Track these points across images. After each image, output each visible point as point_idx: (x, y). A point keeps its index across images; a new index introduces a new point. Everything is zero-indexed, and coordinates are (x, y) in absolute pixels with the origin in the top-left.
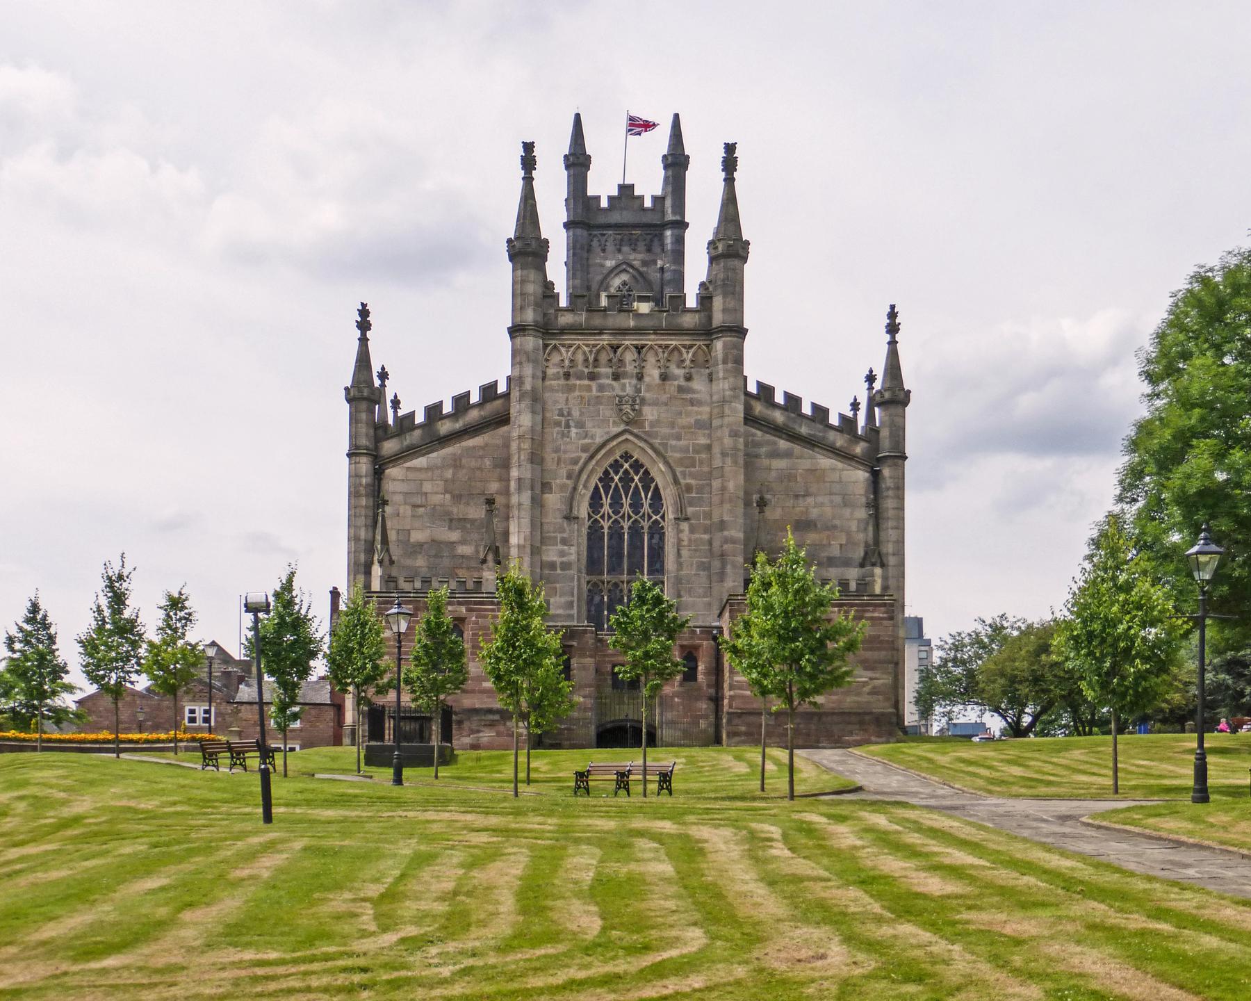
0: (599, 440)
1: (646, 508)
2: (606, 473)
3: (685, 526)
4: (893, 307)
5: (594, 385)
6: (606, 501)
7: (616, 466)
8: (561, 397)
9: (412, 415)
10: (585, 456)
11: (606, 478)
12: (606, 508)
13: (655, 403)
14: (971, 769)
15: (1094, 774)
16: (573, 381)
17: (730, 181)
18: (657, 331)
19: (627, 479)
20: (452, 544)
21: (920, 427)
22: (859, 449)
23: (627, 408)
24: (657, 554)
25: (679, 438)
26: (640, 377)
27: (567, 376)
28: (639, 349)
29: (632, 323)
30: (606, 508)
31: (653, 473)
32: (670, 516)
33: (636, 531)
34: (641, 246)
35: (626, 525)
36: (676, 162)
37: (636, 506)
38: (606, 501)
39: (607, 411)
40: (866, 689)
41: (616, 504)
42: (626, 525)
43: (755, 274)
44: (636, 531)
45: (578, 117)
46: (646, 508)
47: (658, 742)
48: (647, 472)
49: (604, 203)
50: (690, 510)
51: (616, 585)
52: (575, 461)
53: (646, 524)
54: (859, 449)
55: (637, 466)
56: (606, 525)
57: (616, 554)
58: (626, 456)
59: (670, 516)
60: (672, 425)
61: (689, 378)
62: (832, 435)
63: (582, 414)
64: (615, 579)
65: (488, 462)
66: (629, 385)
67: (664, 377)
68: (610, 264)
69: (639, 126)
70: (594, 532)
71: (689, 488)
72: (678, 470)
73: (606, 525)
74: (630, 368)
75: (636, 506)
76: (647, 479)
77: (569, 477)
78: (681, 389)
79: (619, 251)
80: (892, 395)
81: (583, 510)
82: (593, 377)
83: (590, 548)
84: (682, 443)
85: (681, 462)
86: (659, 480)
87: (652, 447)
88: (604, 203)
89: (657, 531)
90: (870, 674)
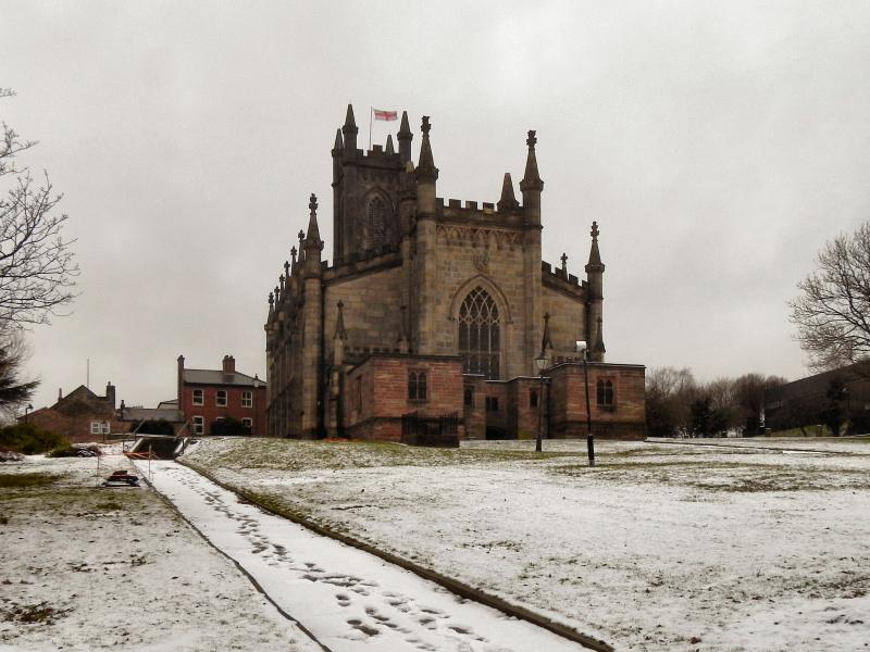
0: (466, 279)
1: (490, 316)
2: (468, 296)
3: (511, 326)
4: (595, 223)
5: (463, 249)
6: (469, 311)
7: (474, 293)
8: (446, 254)
9: (326, 262)
10: (458, 287)
11: (468, 299)
12: (469, 315)
13: (494, 261)
14: (631, 460)
15: (849, 455)
16: (451, 247)
17: (532, 150)
18: (497, 224)
19: (479, 300)
20: (365, 331)
21: (608, 281)
22: (579, 293)
23: (481, 263)
24: (496, 340)
25: (507, 280)
26: (487, 247)
27: (448, 243)
28: (487, 232)
29: (483, 219)
30: (469, 315)
31: (494, 298)
32: (502, 320)
33: (484, 326)
34: (386, 179)
35: (480, 324)
36: (405, 136)
37: (484, 314)
38: (469, 311)
39: (469, 264)
40: (632, 412)
41: (474, 312)
42: (480, 324)
43: (546, 198)
44: (484, 326)
45: (350, 107)
46: (490, 316)
47: (520, 433)
48: (490, 298)
49: (365, 154)
50: (513, 318)
51: (474, 356)
52: (453, 289)
53: (490, 324)
54: (579, 293)
55: (485, 293)
56: (469, 323)
57: (474, 340)
58: (479, 288)
59: (502, 320)
60: (505, 273)
61: (512, 250)
62: (567, 285)
63: (457, 264)
64: (473, 353)
65: (386, 287)
66: (481, 250)
67: (499, 248)
68: (369, 187)
69: (388, 116)
70: (463, 327)
71: (513, 307)
72: (508, 297)
73: (469, 323)
74: (482, 242)
75: (484, 314)
76: (490, 301)
77: (450, 297)
78: (509, 256)
79: (373, 180)
80: (595, 267)
81: (457, 314)
82: (461, 244)
83: (460, 336)
84: (509, 283)
85: (509, 293)
86: (496, 302)
87: (494, 284)
88: (365, 154)
89: (496, 329)
90: (634, 405)
